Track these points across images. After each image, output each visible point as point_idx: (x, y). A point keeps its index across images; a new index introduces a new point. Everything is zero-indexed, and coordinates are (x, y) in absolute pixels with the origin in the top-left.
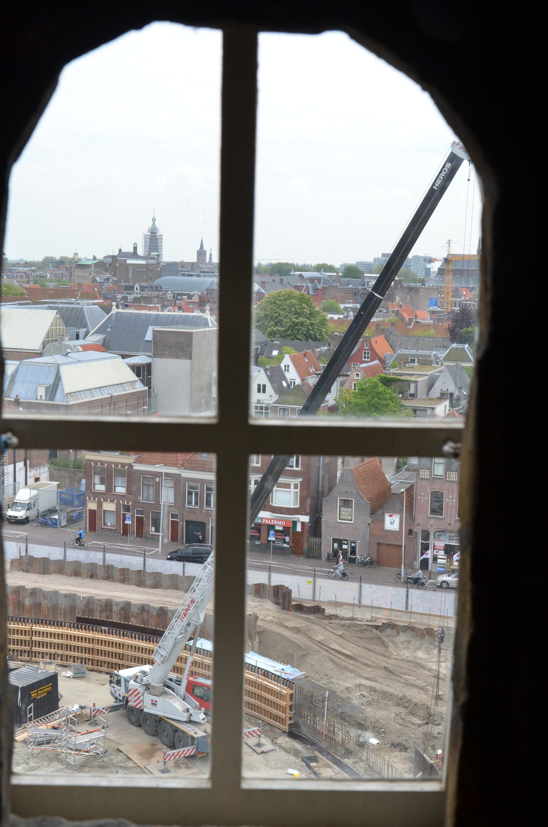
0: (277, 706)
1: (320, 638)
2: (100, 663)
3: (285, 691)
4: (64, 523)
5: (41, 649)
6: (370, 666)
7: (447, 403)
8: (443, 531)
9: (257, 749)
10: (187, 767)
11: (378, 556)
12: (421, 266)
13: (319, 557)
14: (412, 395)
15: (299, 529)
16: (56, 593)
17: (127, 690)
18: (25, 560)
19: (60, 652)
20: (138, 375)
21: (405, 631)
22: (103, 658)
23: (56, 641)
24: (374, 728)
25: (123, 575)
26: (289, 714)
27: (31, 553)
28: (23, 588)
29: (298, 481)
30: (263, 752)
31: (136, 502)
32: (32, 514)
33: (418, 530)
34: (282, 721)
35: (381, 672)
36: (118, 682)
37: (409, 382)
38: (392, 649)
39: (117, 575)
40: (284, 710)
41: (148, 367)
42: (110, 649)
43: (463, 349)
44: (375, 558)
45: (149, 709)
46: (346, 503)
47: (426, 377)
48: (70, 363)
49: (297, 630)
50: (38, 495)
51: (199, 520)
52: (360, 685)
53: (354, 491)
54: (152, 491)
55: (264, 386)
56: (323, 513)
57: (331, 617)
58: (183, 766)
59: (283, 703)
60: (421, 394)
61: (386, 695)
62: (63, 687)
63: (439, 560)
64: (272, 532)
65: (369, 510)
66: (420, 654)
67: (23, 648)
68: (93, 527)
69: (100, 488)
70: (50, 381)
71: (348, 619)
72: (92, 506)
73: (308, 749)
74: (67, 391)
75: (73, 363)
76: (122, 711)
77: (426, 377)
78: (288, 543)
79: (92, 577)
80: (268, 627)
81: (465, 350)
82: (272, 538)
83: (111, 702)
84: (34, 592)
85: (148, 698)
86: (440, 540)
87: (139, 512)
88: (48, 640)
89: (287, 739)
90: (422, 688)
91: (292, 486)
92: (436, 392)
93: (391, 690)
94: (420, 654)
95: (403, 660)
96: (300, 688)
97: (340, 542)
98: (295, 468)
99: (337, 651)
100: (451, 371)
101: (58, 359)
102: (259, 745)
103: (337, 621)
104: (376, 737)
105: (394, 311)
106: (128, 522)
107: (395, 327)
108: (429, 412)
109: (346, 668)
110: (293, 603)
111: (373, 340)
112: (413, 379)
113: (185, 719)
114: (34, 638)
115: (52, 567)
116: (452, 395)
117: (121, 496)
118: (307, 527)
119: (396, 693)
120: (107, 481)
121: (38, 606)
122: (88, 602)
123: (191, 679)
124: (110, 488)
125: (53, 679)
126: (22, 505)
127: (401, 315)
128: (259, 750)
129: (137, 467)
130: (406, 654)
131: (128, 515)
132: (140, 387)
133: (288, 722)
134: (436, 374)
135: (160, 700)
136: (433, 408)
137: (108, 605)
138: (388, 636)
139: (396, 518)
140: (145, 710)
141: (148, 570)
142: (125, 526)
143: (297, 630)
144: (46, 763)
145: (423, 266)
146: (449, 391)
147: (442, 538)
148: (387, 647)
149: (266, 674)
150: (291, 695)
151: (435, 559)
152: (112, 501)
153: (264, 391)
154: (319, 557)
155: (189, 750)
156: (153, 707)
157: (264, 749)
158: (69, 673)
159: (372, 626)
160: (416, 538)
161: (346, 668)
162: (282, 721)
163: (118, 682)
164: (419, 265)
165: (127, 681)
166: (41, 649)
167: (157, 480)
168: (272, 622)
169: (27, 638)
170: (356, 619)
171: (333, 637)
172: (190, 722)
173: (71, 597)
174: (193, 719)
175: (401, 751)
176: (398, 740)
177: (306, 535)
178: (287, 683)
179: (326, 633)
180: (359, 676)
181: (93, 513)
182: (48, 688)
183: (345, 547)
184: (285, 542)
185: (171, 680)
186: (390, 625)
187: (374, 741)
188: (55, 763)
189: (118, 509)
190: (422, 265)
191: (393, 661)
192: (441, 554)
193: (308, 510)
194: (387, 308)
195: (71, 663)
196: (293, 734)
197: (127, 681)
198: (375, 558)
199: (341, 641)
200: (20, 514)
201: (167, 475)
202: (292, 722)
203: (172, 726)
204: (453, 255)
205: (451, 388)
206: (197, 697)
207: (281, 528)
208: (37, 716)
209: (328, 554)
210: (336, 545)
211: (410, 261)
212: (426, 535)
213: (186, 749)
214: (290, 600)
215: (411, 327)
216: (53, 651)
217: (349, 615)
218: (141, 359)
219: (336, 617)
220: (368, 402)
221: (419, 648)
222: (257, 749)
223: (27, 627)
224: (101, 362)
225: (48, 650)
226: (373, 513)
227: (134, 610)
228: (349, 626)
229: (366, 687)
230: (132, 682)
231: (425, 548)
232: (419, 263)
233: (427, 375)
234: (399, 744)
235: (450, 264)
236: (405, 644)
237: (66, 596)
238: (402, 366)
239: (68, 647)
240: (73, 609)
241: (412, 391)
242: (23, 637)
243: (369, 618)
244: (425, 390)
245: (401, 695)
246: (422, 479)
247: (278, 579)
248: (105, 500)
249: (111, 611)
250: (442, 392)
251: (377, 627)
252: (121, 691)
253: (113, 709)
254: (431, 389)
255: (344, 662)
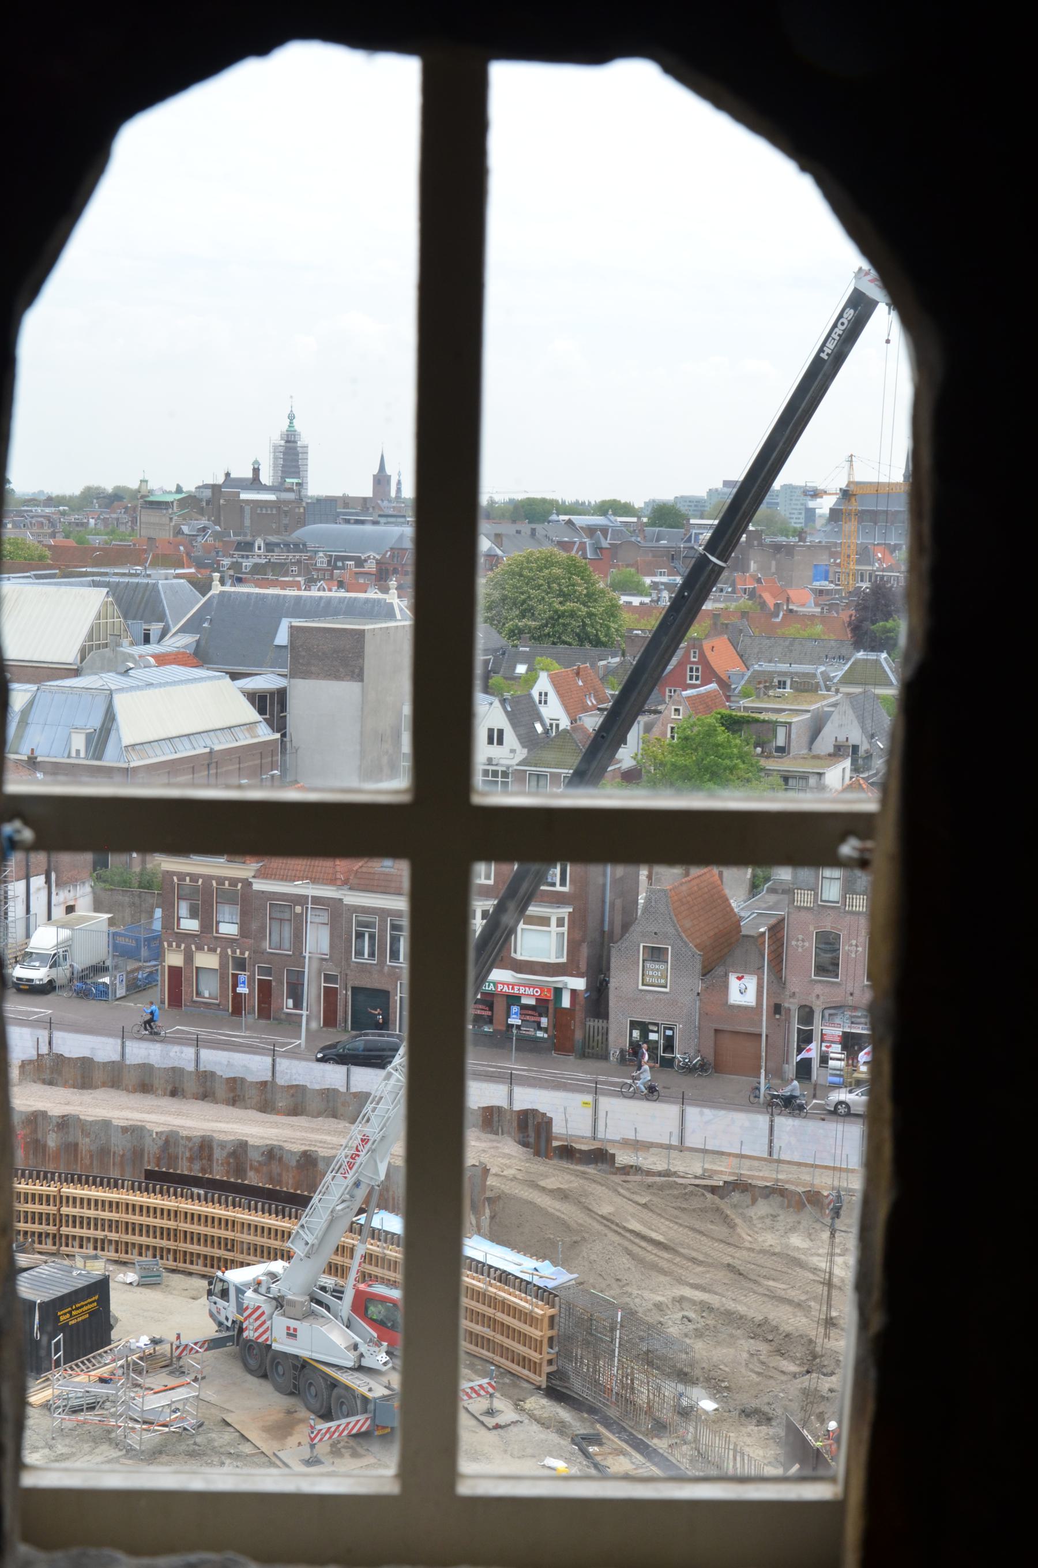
0: (524, 1339)
1: (606, 1209)
2: (189, 1257)
3: (540, 1310)
4: (121, 992)
5: (77, 1231)
6: (700, 1263)
7: (847, 763)
8: (839, 1007)
9: (486, 1420)
10: (355, 1455)
11: (716, 1053)
12: (797, 504)
13: (605, 1057)
14: (781, 750)
15: (566, 1002)
16: (106, 1124)
17: (241, 1308)
18: (47, 1062)
19: (113, 1236)
20: (262, 711)
21: (767, 1197)
22: (195, 1248)
23: (106, 1215)
24: (708, 1380)
25: (233, 1089)
26: (548, 1353)
27: (58, 1048)
28: (44, 1114)
29: (565, 911)
30: (497, 1427)
31: (258, 952)
32: (61, 974)
33: (792, 1005)
34: (534, 1367)
35: (721, 1275)
36: (224, 1294)
37: (775, 724)
38: (742, 1230)
39: (221, 1091)
40: (537, 1346)
41: (281, 695)
42: (209, 1231)
43: (877, 662)
44: (711, 1058)
45: (282, 1345)
46: (656, 954)
47: (808, 716)
48: (132, 688)
49: (562, 1195)
50: (71, 939)
51: (377, 985)
52: (681, 1300)
53: (671, 930)
54: (287, 931)
55: (501, 732)
56: (613, 972)
57: (627, 1170)
58: (347, 1453)
59: (536, 1333)
60: (798, 747)
61: (731, 1318)
62: (119, 1302)
63: (831, 1063)
64: (515, 1009)
65: (699, 966)
66: (796, 1240)
67: (44, 1228)
68: (176, 999)
69: (190, 925)
70: (95, 722)
71: (660, 1174)
72: (174, 959)
73: (583, 1420)
74: (127, 740)
75: (138, 688)
76: (230, 1348)
77: (808, 716)
78: (546, 1030)
79: (174, 1094)
80: (508, 1188)
81: (881, 663)
82: (515, 1020)
83: (210, 1331)
84: (65, 1123)
85: (280, 1324)
86: (833, 1025)
87: (263, 971)
88: (91, 1213)
89: (544, 1401)
90: (799, 1305)
91: (554, 922)
92: (825, 744)
93: (742, 1309)
94: (796, 1240)
95: (763, 1252)
96: (568, 1304)
97: (644, 1028)
98: (558, 888)
99: (638, 1235)
100: (855, 703)
101: (111, 680)
102: (490, 1412)
103: (638, 1178)
104: (713, 1397)
105: (745, 589)
106: (242, 990)
107: (748, 620)
108: (812, 781)
109: (654, 1267)
110: (555, 1144)
111: (706, 645)
112: (782, 718)
113: (350, 1364)
114: (65, 1210)
115: (98, 1076)
116: (855, 748)
117: (230, 941)
118: (581, 1000)
119: (751, 1314)
120: (203, 911)
121: (71, 1149)
122: (167, 1142)
123: (362, 1287)
124: (208, 925)
125: (100, 1288)
126: (42, 958)
127: (760, 596)
128: (490, 1422)
129: (259, 885)
130: (769, 1240)
131: (243, 976)
132: (265, 734)
133: (546, 1369)
134: (826, 709)
135: (303, 1327)
136: (820, 775)
137: (205, 1147)
138: (735, 1206)
139: (751, 983)
140: (275, 1346)
141: (281, 1081)
142: (237, 997)
143: (562, 1195)
144: (86, 1447)
145: (802, 504)
146: (851, 742)
147: (837, 1021)
148: (732, 1226)
149: (504, 1277)
150: (552, 1318)
151: (824, 1059)
152: (212, 950)
153: (500, 742)
154: (605, 1057)
155: (358, 1422)
156: (291, 1341)
157: (500, 1420)
158: (132, 1277)
159: (705, 1187)
160: (788, 1020)
161: (654, 1267)
162: (534, 1367)
163: (224, 1294)
164: (794, 502)
165: (240, 1291)
166: (77, 1231)
167: (298, 909)
168: (514, 1179)
169: (52, 1209)
170: (675, 1174)
171: (631, 1208)
172: (360, 1368)
173: (135, 1131)
174: (365, 1363)
175: (759, 1424)
176: (755, 1404)
177: (579, 1015)
178: (545, 1294)
179: (618, 1200)
180: (680, 1281)
181: (175, 973)
182: (90, 1305)
183: (653, 1036)
184: (540, 1028)
185: (323, 1289)
186: (739, 1186)
187: (708, 1405)
188: (104, 1447)
189: (223, 965)
190: (799, 503)
191: (745, 1253)
192: (836, 1050)
193: (583, 966)
194: (733, 585)
195: (134, 1257)
196: (555, 1393)
197: (240, 1291)
198: (711, 1058)
199: (646, 1215)
200: (39, 974)
201: (316, 900)
202: (553, 1368)
203: (326, 1376)
204: (858, 483)
205: (855, 736)
206: (373, 1322)
207: (532, 1002)
208: (69, 1358)
209: (622, 1051)
210: (636, 1034)
211: (777, 496)
212: (807, 1015)
213: (353, 1419)
214: (549, 1137)
215: (778, 620)
216: (100, 1234)
217: (660, 1166)
218: (266, 681)
219: (636, 1169)
220: (698, 763)
221: (793, 1229)
222: (486, 1420)
223: (52, 1189)
224: (192, 687)
225: (91, 1233)
226: (706, 972)
227: (255, 1156)
228: (661, 1188)
229: (694, 1302)
230: (249, 1293)
231: (806, 1038)
232: (793, 498)
233: (808, 711)
234: (756, 1411)
235: (853, 500)
236: (768, 1221)
237: (125, 1130)
238: (762, 694)
239: (130, 1228)
240: (138, 1154)
241: (781, 741)
242: (44, 1208)
243: (699, 1172)
244: (805, 740)
245: (759, 1317)
246: (799, 908)
247: (527, 1098)
248: (200, 948)
249: (210, 1158)
250: (837, 744)
251: (713, 1189)
252: (229, 1310)
253: (214, 1344)
254: (816, 738)
255: (652, 1255)
